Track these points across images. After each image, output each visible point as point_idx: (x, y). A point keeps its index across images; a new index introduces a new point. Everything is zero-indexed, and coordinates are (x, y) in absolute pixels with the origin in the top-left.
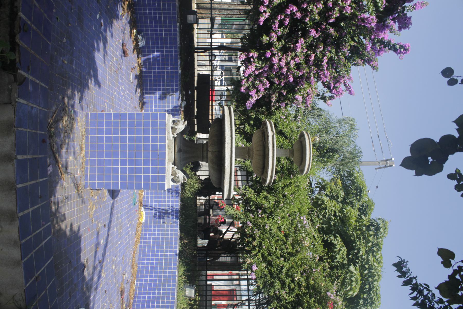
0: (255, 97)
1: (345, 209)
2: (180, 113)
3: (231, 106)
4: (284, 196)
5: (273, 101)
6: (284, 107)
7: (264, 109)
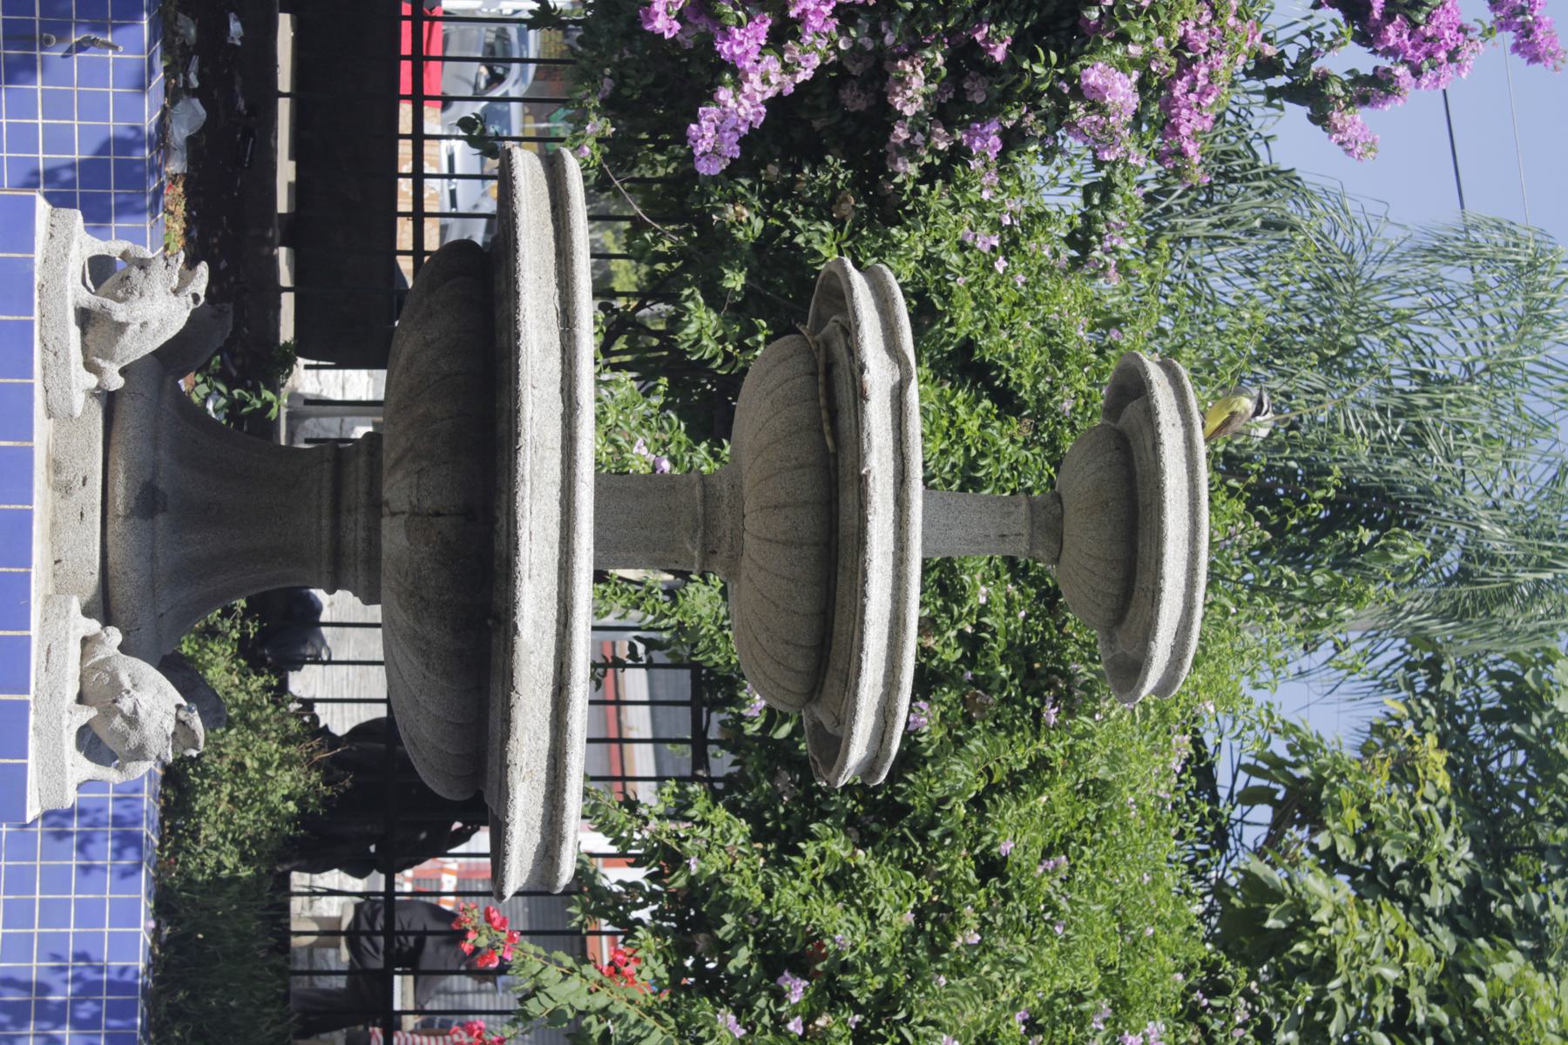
0: (765, 80)
1: (1481, 975)
2: (158, 193)
3: (566, 152)
4: (991, 867)
5: (909, 111)
6: (992, 156)
7: (835, 171)
